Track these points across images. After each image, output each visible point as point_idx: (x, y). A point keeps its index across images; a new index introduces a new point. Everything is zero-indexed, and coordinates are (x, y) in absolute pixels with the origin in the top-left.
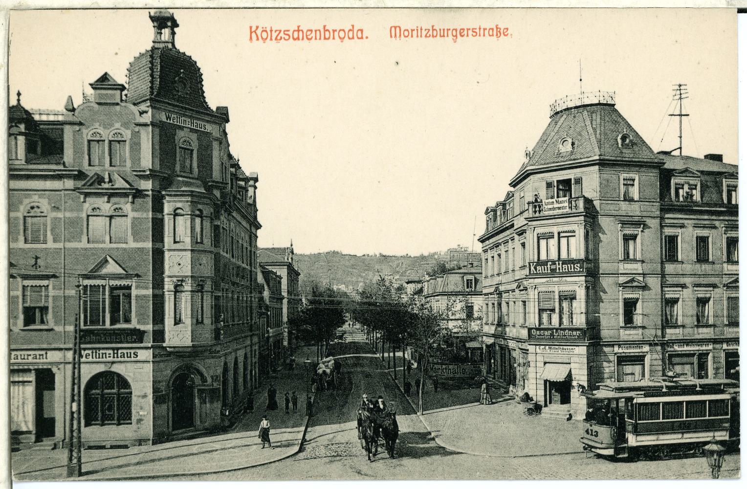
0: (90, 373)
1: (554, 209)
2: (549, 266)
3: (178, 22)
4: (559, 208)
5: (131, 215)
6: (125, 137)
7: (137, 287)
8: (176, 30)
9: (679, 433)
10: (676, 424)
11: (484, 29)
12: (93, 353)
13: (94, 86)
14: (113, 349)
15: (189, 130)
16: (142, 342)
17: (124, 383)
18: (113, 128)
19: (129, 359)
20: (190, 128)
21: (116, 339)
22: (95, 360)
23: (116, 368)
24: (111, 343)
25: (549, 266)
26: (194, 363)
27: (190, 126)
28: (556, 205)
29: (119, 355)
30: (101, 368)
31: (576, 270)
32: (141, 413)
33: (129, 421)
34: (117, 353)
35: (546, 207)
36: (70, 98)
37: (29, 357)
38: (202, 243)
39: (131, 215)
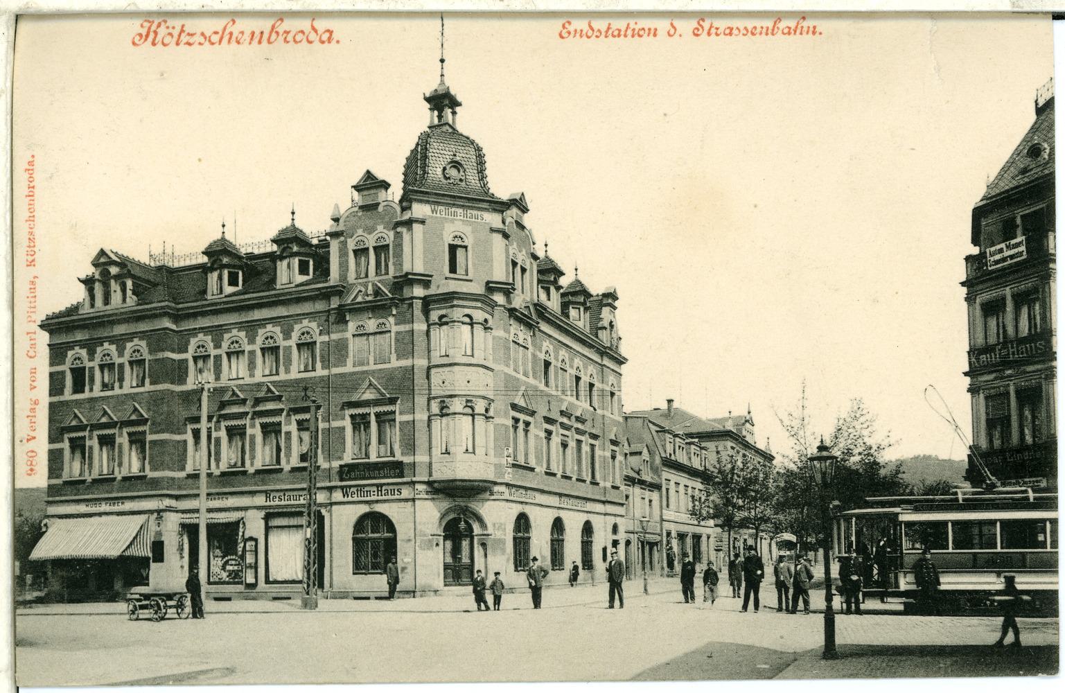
0: (356, 513)
1: (1004, 260)
2: (997, 352)
3: (459, 99)
4: (1012, 257)
5: (394, 329)
6: (466, 241)
7: (401, 413)
8: (458, 109)
9: (992, 572)
10: (1020, 564)
11: (761, 33)
12: (357, 490)
13: (357, 188)
14: (377, 485)
15: (461, 223)
16: (403, 477)
17: (391, 527)
18: (376, 232)
19: (393, 497)
20: (463, 221)
21: (379, 474)
22: (360, 499)
23: (379, 508)
24: (375, 478)
25: (997, 352)
26: (469, 505)
27: (462, 218)
28: (1007, 253)
29: (383, 492)
30: (364, 509)
31: (1039, 351)
32: (406, 560)
33: (195, 492)
34: (381, 491)
35: (992, 259)
36: (337, 206)
37: (301, 498)
38: (472, 356)
39: (394, 329)
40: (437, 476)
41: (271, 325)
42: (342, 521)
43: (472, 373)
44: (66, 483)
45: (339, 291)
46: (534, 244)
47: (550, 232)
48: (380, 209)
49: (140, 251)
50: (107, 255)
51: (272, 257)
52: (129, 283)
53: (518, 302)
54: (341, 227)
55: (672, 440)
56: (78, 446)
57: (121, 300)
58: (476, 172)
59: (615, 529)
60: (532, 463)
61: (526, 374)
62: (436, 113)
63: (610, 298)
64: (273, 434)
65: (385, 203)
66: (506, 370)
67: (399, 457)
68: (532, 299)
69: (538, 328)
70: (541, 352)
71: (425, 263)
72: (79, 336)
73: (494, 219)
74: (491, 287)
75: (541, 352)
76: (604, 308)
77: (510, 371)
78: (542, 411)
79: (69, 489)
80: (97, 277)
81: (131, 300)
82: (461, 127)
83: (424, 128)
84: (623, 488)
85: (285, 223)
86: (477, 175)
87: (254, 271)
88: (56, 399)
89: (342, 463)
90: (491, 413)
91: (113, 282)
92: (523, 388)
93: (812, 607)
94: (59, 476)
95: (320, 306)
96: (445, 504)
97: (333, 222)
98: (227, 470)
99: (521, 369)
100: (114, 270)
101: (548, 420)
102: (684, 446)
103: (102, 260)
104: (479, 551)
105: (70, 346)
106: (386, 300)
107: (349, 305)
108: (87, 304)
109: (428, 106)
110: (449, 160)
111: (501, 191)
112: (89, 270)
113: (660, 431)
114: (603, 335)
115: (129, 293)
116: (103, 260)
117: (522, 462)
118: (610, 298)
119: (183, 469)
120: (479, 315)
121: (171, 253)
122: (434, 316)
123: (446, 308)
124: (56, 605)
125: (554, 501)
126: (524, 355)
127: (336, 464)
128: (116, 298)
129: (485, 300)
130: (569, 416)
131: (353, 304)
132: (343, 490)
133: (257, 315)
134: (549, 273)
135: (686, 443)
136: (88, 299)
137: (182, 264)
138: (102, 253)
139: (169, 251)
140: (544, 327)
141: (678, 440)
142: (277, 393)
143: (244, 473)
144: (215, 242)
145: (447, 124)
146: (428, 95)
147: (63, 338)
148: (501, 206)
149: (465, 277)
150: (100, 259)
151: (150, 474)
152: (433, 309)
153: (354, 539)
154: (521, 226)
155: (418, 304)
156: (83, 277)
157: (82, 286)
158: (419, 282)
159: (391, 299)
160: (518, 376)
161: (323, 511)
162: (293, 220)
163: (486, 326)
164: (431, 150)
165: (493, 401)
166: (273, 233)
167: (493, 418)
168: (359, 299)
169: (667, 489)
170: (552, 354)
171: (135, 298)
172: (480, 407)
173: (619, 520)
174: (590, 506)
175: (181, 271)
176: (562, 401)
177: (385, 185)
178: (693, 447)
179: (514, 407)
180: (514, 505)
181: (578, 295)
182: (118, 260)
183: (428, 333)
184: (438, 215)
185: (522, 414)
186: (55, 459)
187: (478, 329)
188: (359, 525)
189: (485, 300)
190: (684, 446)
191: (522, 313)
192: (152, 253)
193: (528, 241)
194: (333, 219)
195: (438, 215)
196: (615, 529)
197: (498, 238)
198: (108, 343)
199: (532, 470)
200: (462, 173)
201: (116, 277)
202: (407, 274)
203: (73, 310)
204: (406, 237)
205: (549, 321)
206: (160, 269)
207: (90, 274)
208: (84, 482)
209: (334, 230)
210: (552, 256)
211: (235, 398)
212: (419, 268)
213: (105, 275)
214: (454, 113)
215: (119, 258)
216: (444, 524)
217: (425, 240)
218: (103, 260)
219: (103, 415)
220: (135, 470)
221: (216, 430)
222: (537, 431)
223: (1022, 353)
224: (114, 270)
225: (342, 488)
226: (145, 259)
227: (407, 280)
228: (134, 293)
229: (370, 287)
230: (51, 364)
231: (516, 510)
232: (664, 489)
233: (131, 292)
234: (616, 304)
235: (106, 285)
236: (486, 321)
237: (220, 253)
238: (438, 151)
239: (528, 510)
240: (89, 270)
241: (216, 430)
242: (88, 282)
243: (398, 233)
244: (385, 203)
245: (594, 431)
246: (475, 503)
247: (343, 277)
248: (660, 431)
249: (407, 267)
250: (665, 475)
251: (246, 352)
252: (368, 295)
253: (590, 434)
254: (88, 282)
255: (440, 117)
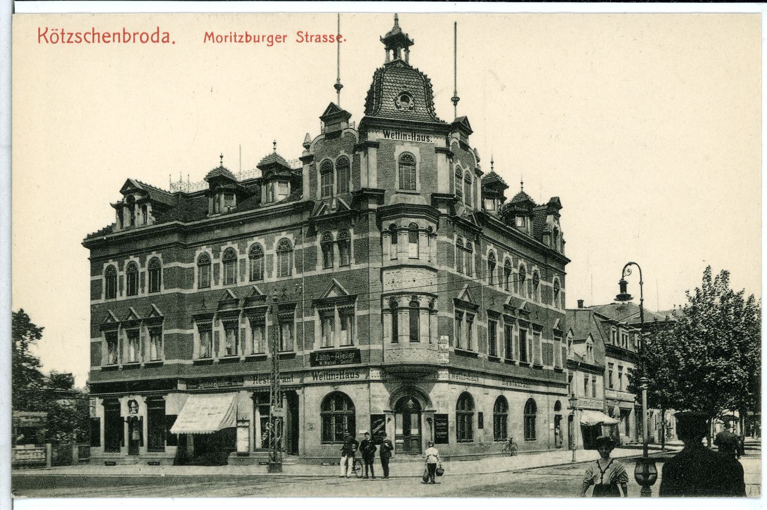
8: (410, 48)
17: (351, 404)
23: (344, 389)
30: (328, 390)
40: (387, 362)
41: (257, 238)
42: (311, 400)
43: (414, 273)
44: (104, 369)
45: (309, 205)
46: (478, 161)
47: (493, 150)
48: (343, 135)
49: (161, 179)
50: (132, 184)
51: (259, 182)
52: (149, 208)
53: (462, 211)
54: (312, 152)
55: (615, 330)
56: (112, 340)
57: (144, 219)
58: (423, 100)
59: (558, 406)
60: (475, 349)
61: (468, 274)
62: (392, 52)
63: (554, 206)
64: (259, 329)
65: (346, 131)
66: (450, 270)
67: (357, 346)
68: (476, 209)
69: (482, 233)
70: (485, 255)
71: (378, 180)
72: (113, 251)
73: (440, 142)
74: (436, 199)
75: (485, 255)
76: (548, 216)
77: (454, 271)
78: (485, 304)
79: (106, 373)
80: (125, 202)
81: (151, 219)
82: (413, 62)
83: (380, 64)
84: (566, 371)
85: (269, 151)
86: (424, 103)
87: (246, 193)
88: (96, 302)
89: (312, 351)
90: (435, 308)
91: (136, 206)
92: (466, 286)
93: (376, 474)
94: (98, 364)
95: (295, 219)
96: (396, 386)
97: (305, 149)
98: (200, 360)
99: (465, 270)
100: (137, 197)
101: (491, 313)
102: (628, 335)
103: (129, 188)
104: (426, 425)
105: (106, 258)
106: (347, 212)
107: (318, 218)
108: (118, 228)
109: (384, 46)
110: (400, 91)
111: (445, 113)
112: (120, 197)
113: (606, 322)
114: (547, 241)
115: (149, 214)
116: (129, 188)
117: (464, 347)
118: (554, 206)
119: (191, 358)
120: (423, 223)
121: (186, 182)
122: (386, 225)
123: (394, 218)
124: (194, 467)
125: (500, 383)
126: (469, 258)
127: (308, 352)
128: (139, 220)
129: (429, 211)
130: (513, 310)
131: (321, 217)
132: (313, 373)
133: (246, 229)
134: (494, 187)
135: (630, 332)
136: (119, 221)
137: (195, 190)
138: (129, 183)
139: (185, 179)
140: (487, 232)
141: (621, 329)
142: (262, 294)
143: (238, 360)
144: (214, 170)
145: (402, 62)
146: (383, 37)
147: (100, 253)
148: (442, 129)
149: (413, 192)
150: (127, 187)
151: (166, 362)
152: (385, 220)
153: (322, 415)
154: (465, 147)
155: (372, 218)
156: (115, 202)
157: (114, 210)
158: (372, 196)
159: (350, 211)
160: (462, 275)
161: (298, 392)
162: (522, 188)
163: (430, 233)
164: (384, 84)
165: (436, 297)
166: (258, 161)
167: (437, 311)
168: (326, 213)
169: (611, 372)
170: (496, 256)
171: (154, 219)
172: (424, 302)
173: (561, 399)
174: (533, 388)
175: (195, 196)
176: (505, 296)
177: (346, 116)
178: (636, 335)
179: (458, 302)
180: (457, 386)
181: (524, 205)
182: (141, 188)
183: (381, 239)
184: (390, 138)
185: (465, 308)
186: (95, 348)
187: (423, 238)
188: (326, 403)
189: (429, 211)
190: (628, 335)
191: (465, 221)
192: (172, 182)
193: (471, 156)
194: (305, 147)
195: (390, 138)
196: (558, 406)
197: (442, 157)
198: (133, 256)
199: (475, 356)
200: (411, 102)
201: (139, 202)
202: (364, 189)
203: (108, 230)
204: (363, 159)
205: (490, 227)
206: (177, 194)
207: (120, 200)
208: (117, 368)
209: (306, 154)
210: (497, 171)
211: (229, 299)
212: (374, 185)
213: (130, 200)
214: (407, 51)
215: (142, 186)
216: (394, 404)
217: (379, 164)
218: (129, 188)
219: (130, 315)
220: (154, 357)
221: (215, 326)
222: (481, 323)
223: (407, 160)
224: (137, 197)
225: (313, 371)
226: (165, 187)
227: (362, 196)
228: (153, 214)
229: (334, 203)
230: (92, 275)
231: (458, 390)
232: (607, 373)
233: (151, 214)
234: (561, 212)
235: (132, 210)
236: (430, 228)
237: (220, 181)
238: (391, 84)
239: (472, 391)
240: (120, 197)
241: (215, 326)
242: (118, 207)
243: (357, 155)
244: (346, 131)
245: (537, 322)
246: (423, 385)
247: (313, 194)
248: (606, 322)
249: (364, 184)
250: (608, 360)
251: (238, 260)
252: (333, 210)
253: (534, 325)
254: (118, 207)
255: (395, 55)
